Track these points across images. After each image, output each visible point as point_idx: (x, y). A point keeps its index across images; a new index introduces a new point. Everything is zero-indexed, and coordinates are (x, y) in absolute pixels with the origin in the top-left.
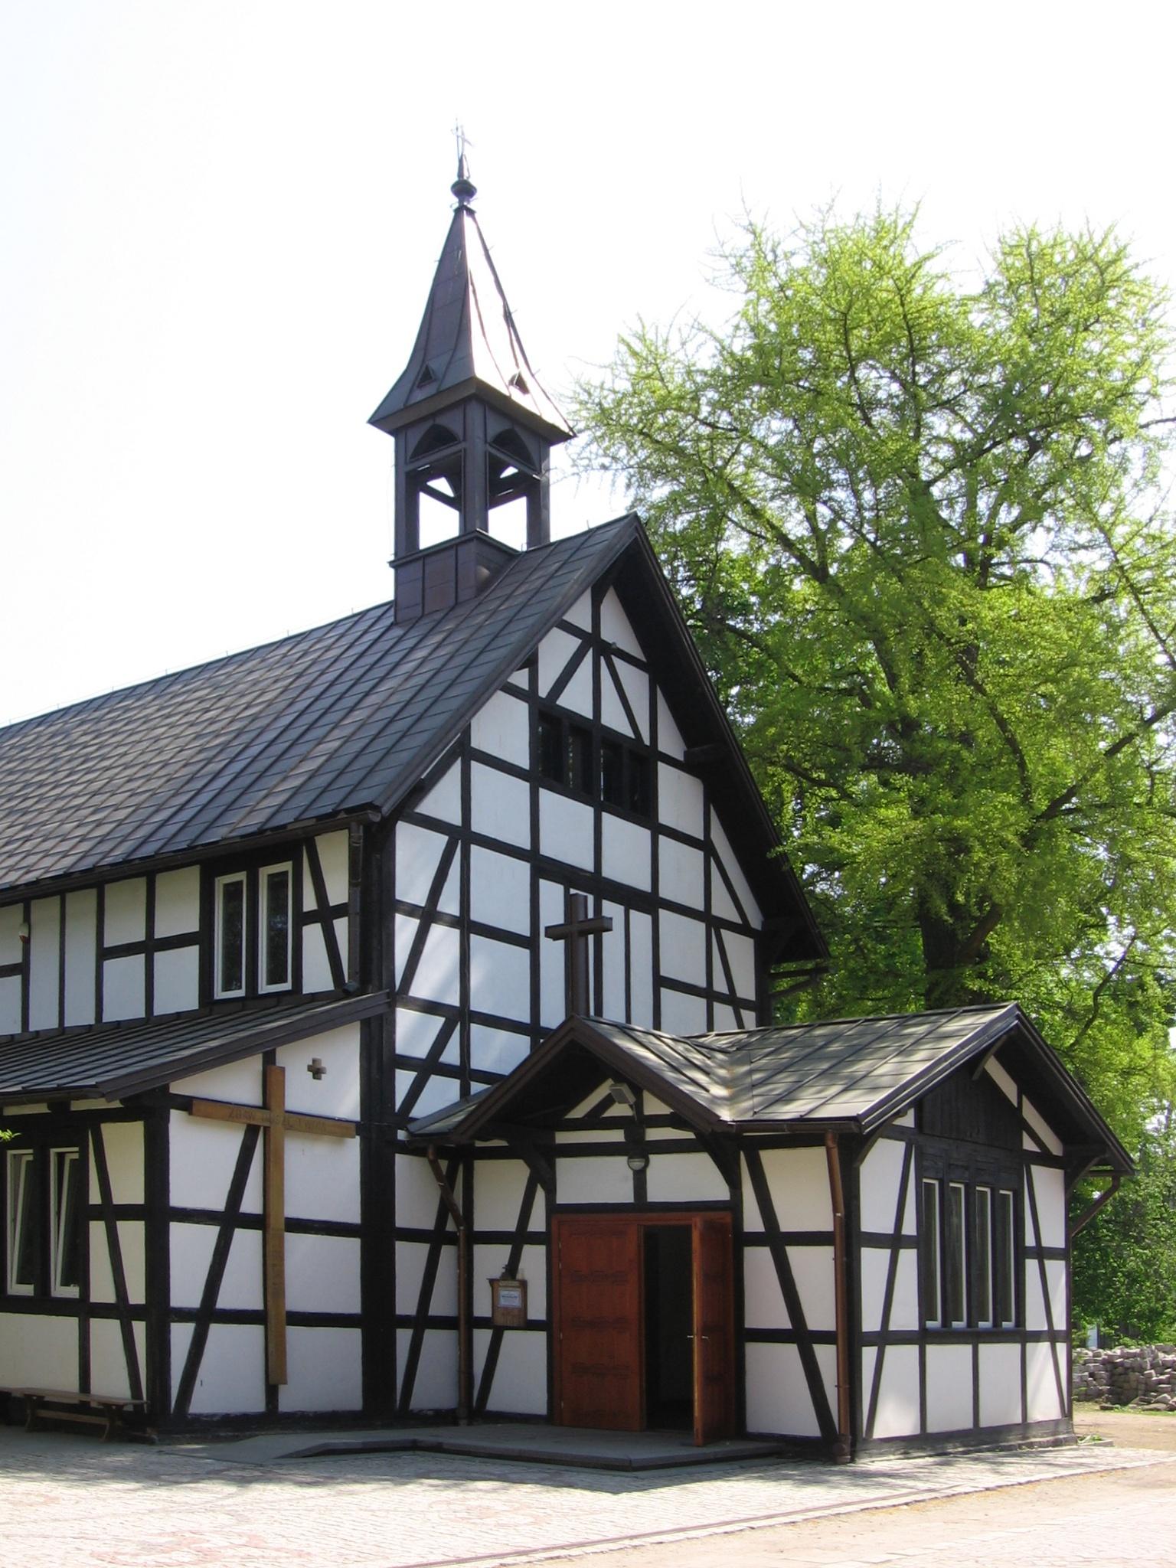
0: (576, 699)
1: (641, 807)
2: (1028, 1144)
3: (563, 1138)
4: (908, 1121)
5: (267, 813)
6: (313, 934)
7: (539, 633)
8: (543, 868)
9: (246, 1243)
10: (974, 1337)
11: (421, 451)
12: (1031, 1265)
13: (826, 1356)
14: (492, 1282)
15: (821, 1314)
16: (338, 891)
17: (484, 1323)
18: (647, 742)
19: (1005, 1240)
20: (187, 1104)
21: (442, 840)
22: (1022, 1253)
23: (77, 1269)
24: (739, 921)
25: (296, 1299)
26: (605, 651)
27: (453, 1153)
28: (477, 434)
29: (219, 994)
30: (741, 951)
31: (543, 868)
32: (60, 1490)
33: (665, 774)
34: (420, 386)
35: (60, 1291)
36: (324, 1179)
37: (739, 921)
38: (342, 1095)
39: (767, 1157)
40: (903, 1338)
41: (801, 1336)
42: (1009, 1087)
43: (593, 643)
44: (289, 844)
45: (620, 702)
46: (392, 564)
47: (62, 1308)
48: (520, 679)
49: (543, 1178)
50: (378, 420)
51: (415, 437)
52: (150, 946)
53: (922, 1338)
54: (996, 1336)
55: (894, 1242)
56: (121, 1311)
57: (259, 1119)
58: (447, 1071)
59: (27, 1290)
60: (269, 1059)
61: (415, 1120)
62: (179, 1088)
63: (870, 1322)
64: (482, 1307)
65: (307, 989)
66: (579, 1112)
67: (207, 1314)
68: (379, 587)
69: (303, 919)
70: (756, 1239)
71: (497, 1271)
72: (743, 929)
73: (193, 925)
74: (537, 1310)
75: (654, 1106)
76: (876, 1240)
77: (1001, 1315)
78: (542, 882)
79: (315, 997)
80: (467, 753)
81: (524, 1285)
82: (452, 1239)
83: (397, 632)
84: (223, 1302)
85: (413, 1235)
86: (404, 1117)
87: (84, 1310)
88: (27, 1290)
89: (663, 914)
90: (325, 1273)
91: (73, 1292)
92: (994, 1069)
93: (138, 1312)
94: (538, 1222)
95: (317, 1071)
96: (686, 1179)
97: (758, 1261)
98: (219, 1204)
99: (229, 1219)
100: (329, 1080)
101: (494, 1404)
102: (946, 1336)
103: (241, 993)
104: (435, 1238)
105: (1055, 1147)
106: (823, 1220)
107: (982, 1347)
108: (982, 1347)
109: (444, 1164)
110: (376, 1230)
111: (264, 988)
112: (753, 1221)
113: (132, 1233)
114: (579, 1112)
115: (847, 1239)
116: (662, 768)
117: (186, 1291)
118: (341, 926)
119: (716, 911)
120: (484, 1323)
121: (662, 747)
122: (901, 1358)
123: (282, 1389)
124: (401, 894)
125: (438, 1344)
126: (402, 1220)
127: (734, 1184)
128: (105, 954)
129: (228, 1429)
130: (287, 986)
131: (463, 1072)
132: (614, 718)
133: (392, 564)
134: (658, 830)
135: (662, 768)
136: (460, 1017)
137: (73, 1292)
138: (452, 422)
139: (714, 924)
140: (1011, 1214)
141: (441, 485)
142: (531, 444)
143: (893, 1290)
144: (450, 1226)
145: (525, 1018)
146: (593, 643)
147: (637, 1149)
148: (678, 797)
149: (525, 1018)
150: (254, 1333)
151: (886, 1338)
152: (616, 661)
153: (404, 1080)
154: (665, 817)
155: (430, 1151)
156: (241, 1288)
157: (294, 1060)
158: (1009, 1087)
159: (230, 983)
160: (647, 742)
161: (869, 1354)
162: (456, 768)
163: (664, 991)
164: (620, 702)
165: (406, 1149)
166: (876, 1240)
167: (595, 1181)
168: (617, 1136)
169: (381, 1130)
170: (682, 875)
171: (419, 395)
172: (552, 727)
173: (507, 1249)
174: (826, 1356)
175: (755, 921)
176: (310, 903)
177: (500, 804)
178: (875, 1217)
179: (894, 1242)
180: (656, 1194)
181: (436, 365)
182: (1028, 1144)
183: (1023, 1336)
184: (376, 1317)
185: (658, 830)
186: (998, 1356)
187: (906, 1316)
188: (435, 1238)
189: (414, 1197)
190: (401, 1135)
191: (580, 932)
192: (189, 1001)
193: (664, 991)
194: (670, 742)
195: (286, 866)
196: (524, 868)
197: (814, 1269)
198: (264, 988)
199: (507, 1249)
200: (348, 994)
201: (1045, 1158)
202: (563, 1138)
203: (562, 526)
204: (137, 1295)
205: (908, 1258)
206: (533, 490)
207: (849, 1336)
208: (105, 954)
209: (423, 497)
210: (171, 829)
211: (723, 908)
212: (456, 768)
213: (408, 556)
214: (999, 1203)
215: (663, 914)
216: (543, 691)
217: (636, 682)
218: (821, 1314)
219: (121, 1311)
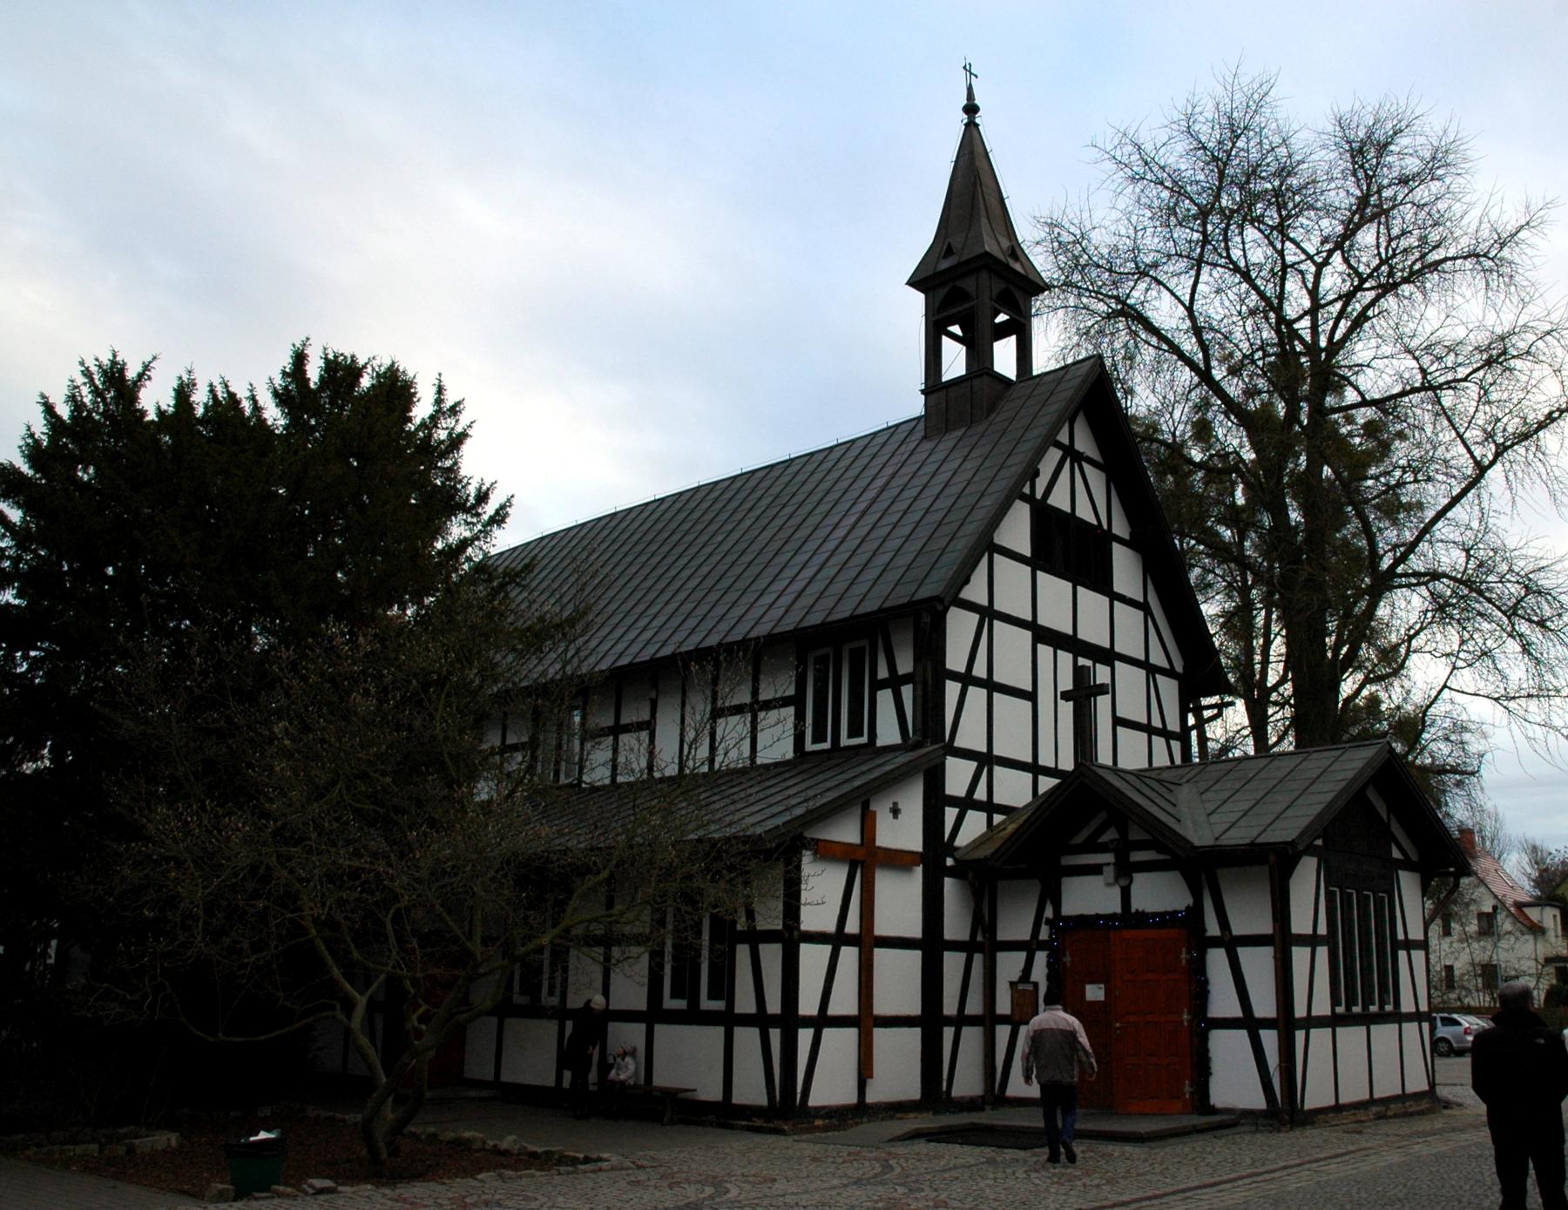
0: (1059, 499)
1: (1101, 581)
2: (1396, 854)
3: (1068, 860)
5: (856, 600)
6: (885, 698)
7: (1040, 454)
10: (1367, 1020)
11: (943, 306)
12: (1402, 954)
13: (1269, 1038)
14: (1012, 984)
15: (1264, 1006)
16: (905, 665)
18: (1105, 527)
19: (1368, 933)
21: (975, 617)
22: (1329, 940)
23: (723, 985)
24: (1167, 666)
25: (881, 1007)
27: (985, 876)
28: (983, 287)
29: (809, 746)
30: (1169, 688)
31: (1042, 635)
32: (1111, 1147)
33: (1118, 550)
34: (945, 257)
35: (706, 1004)
36: (899, 904)
37: (1167, 666)
40: (1321, 1022)
45: (1083, 496)
46: (923, 392)
47: (709, 1019)
49: (1052, 894)
50: (914, 282)
51: (941, 293)
52: (756, 708)
53: (1333, 1021)
54: (1382, 1018)
55: (1312, 941)
56: (761, 1020)
58: (978, 806)
59: (681, 1004)
60: (616, 740)
61: (957, 849)
63: (1300, 1011)
65: (879, 743)
66: (1079, 839)
68: (913, 405)
69: (877, 685)
70: (1215, 942)
71: (1015, 975)
72: (1170, 673)
73: (791, 691)
75: (1136, 834)
77: (1351, 1002)
78: (1040, 646)
81: (1036, 985)
83: (928, 445)
84: (832, 1010)
85: (955, 946)
86: (950, 848)
87: (729, 1020)
88: (681, 1004)
89: (1117, 664)
91: (719, 1005)
92: (1372, 795)
93: (773, 1021)
94: (1044, 934)
96: (1158, 893)
97: (1217, 960)
98: (831, 927)
100: (902, 829)
102: (1348, 1020)
103: (827, 745)
106: (1265, 927)
107: (1373, 1028)
108: (1373, 1028)
110: (931, 944)
111: (845, 741)
112: (1213, 929)
113: (772, 955)
114: (1079, 839)
115: (1282, 940)
116: (1116, 547)
117: (808, 1005)
118: (907, 692)
119: (1152, 660)
121: (1116, 531)
122: (1320, 1036)
123: (869, 1081)
124: (950, 665)
125: (972, 1037)
126: (949, 934)
128: (717, 714)
129: (839, 1117)
130: (864, 740)
131: (989, 807)
132: (1084, 512)
133: (923, 392)
134: (1114, 597)
135: (1116, 547)
136: (986, 760)
137: (719, 1005)
138: (969, 284)
139: (1151, 670)
141: (956, 329)
142: (1018, 295)
144: (979, 938)
145: (1029, 759)
147: (1125, 872)
148: (1126, 570)
149: (1029, 759)
150: (852, 1033)
151: (1311, 1022)
152: (1085, 465)
153: (951, 814)
154: (1117, 588)
155: (970, 875)
159: (819, 737)
160: (1105, 527)
161: (1300, 1035)
162: (985, 560)
163: (1119, 729)
164: (1083, 496)
165: (951, 873)
167: (1090, 896)
168: (1108, 858)
170: (1130, 633)
171: (944, 265)
172: (1047, 521)
173: (1022, 955)
174: (1269, 1038)
175: (1179, 668)
176: (883, 673)
177: (1011, 585)
178: (1301, 923)
179: (1312, 941)
180: (1137, 904)
181: (957, 242)
182: (1396, 854)
183: (1398, 1017)
184: (930, 1020)
185: (1114, 597)
186: (1384, 1034)
187: (1322, 1007)
190: (949, 862)
191: (1083, 694)
192: (785, 750)
193: (1119, 729)
194: (1120, 528)
195: (865, 643)
196: (1028, 635)
197: (1258, 964)
198: (845, 741)
199: (1022, 955)
200: (917, 746)
201: (1407, 865)
202: (1068, 860)
203: (1043, 362)
204: (774, 1006)
205: (1322, 952)
206: (1021, 330)
207: (1286, 1023)
209: (945, 339)
211: (1158, 658)
212: (985, 560)
213: (934, 385)
214: (1379, 904)
215: (1117, 664)
216: (1039, 496)
217: (1096, 478)
218: (1264, 1006)
219: (761, 1020)
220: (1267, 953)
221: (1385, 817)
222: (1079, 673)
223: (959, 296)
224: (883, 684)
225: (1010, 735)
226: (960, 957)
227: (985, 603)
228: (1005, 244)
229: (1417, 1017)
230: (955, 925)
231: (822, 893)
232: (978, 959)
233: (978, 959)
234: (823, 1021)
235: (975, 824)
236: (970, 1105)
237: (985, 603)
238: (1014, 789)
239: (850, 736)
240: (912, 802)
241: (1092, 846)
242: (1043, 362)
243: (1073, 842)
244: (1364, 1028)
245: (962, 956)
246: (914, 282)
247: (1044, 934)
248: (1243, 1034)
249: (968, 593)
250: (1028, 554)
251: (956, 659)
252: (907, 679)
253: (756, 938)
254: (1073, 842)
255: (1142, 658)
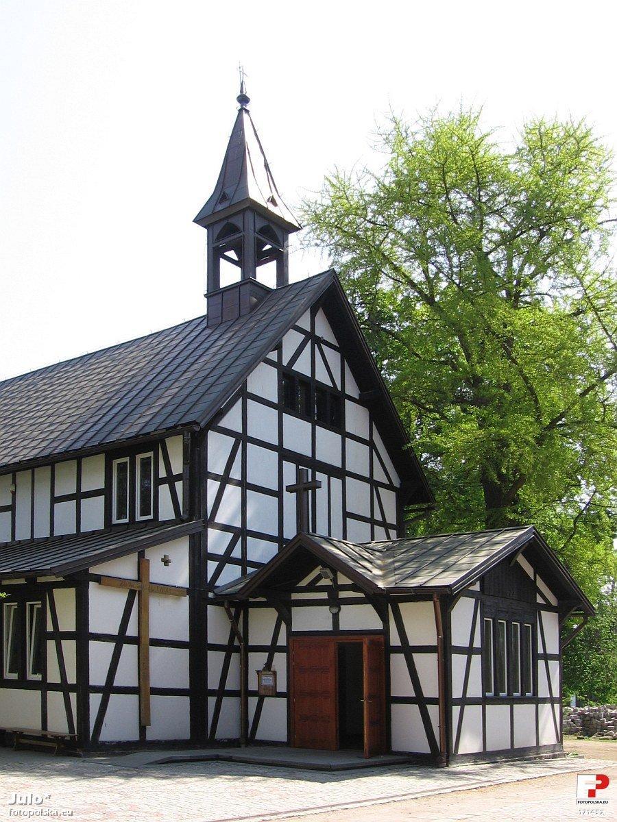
1: (335, 422)
3: (296, 596)
4: (477, 588)
6: (164, 490)
7: (283, 332)
8: (285, 455)
9: (129, 651)
10: (511, 701)
11: (221, 236)
12: (541, 663)
13: (434, 711)
14: (258, 672)
16: (178, 467)
17: (254, 693)
20: (98, 579)
23: (41, 666)
25: (156, 681)
26: (317, 341)
27: (238, 605)
28: (251, 227)
29: (115, 521)
30: (389, 499)
31: (285, 455)
36: (170, 618)
38: (180, 575)
39: (402, 606)
40: (474, 701)
41: (420, 700)
42: (529, 570)
43: (311, 337)
44: (152, 442)
45: (325, 368)
48: (273, 356)
49: (285, 617)
50: (197, 221)
51: (218, 229)
52: (79, 496)
53: (484, 701)
54: (523, 700)
55: (469, 651)
56: (64, 687)
57: (136, 586)
58: (235, 561)
59: (15, 676)
60: (141, 555)
62: (94, 570)
64: (253, 686)
66: (304, 583)
67: (109, 689)
68: (198, 307)
69: (158, 482)
70: (396, 650)
71: (261, 667)
72: (390, 487)
74: (282, 687)
75: (343, 580)
76: (460, 650)
77: (525, 689)
79: (165, 523)
80: (245, 395)
81: (275, 673)
82: (237, 650)
83: (208, 331)
84: (117, 682)
86: (212, 586)
87: (44, 687)
88: (15, 676)
90: (170, 667)
91: (38, 677)
92: (521, 560)
93: (72, 688)
94: (282, 641)
95: (166, 562)
97: (398, 660)
98: (115, 632)
99: (120, 639)
101: (259, 736)
102: (496, 700)
104: (228, 649)
105: (554, 601)
106: (432, 640)
109: (233, 610)
110: (197, 645)
111: (139, 518)
112: (395, 640)
113: (70, 647)
115: (444, 649)
117: (97, 676)
118: (179, 486)
120: (254, 693)
122: (473, 712)
126: (212, 639)
127: (385, 621)
128: (55, 500)
130: (151, 517)
131: (243, 562)
132: (322, 377)
134: (346, 436)
137: (38, 677)
138: (237, 221)
139: (375, 484)
140: (531, 636)
143: (468, 675)
144: (236, 643)
146: (311, 337)
148: (356, 418)
151: (464, 701)
153: (212, 566)
156: (127, 675)
157: (154, 556)
158: (529, 570)
159: (121, 514)
161: (456, 710)
162: (240, 402)
164: (325, 368)
165: (212, 602)
166: (460, 650)
169: (200, 592)
170: (358, 458)
171: (220, 207)
174: (434, 711)
176: (162, 473)
177: (262, 422)
178: (460, 637)
179: (469, 651)
182: (540, 600)
183: (536, 701)
184: (197, 691)
185: (346, 436)
186: (524, 711)
187: (475, 690)
188: (228, 649)
189: (217, 627)
191: (304, 489)
192: (99, 525)
194: (352, 389)
196: (275, 455)
197: (427, 665)
198: (139, 518)
200: (182, 521)
201: (548, 607)
202: (296, 596)
203: (294, 276)
204: (72, 679)
205: (477, 659)
207: (446, 700)
208: (55, 500)
209: (222, 260)
210: (89, 435)
211: (379, 476)
212: (240, 402)
213: (214, 291)
214: (524, 631)
216: (285, 363)
217: (333, 357)
218: (431, 688)
220: (433, 657)
221: (539, 579)
222: (299, 473)
223: (230, 229)
224: (163, 481)
225: (246, 511)
226: (221, 655)
227: (240, 430)
228: (267, 195)
229: (552, 701)
230: (217, 627)
231: (106, 609)
232: (235, 657)
233: (235, 657)
234: (221, 693)
235: (231, 574)
236: (231, 743)
237: (240, 430)
238: (262, 552)
239: (142, 515)
240: (180, 553)
241: (312, 587)
242: (294, 276)
243: (299, 585)
244: (508, 707)
245: (222, 655)
246: (197, 221)
247: (282, 641)
248: (416, 708)
249: (225, 423)
250: (276, 401)
251: (216, 464)
252: (179, 478)
253: (59, 636)
254: (299, 585)
255: (368, 476)
